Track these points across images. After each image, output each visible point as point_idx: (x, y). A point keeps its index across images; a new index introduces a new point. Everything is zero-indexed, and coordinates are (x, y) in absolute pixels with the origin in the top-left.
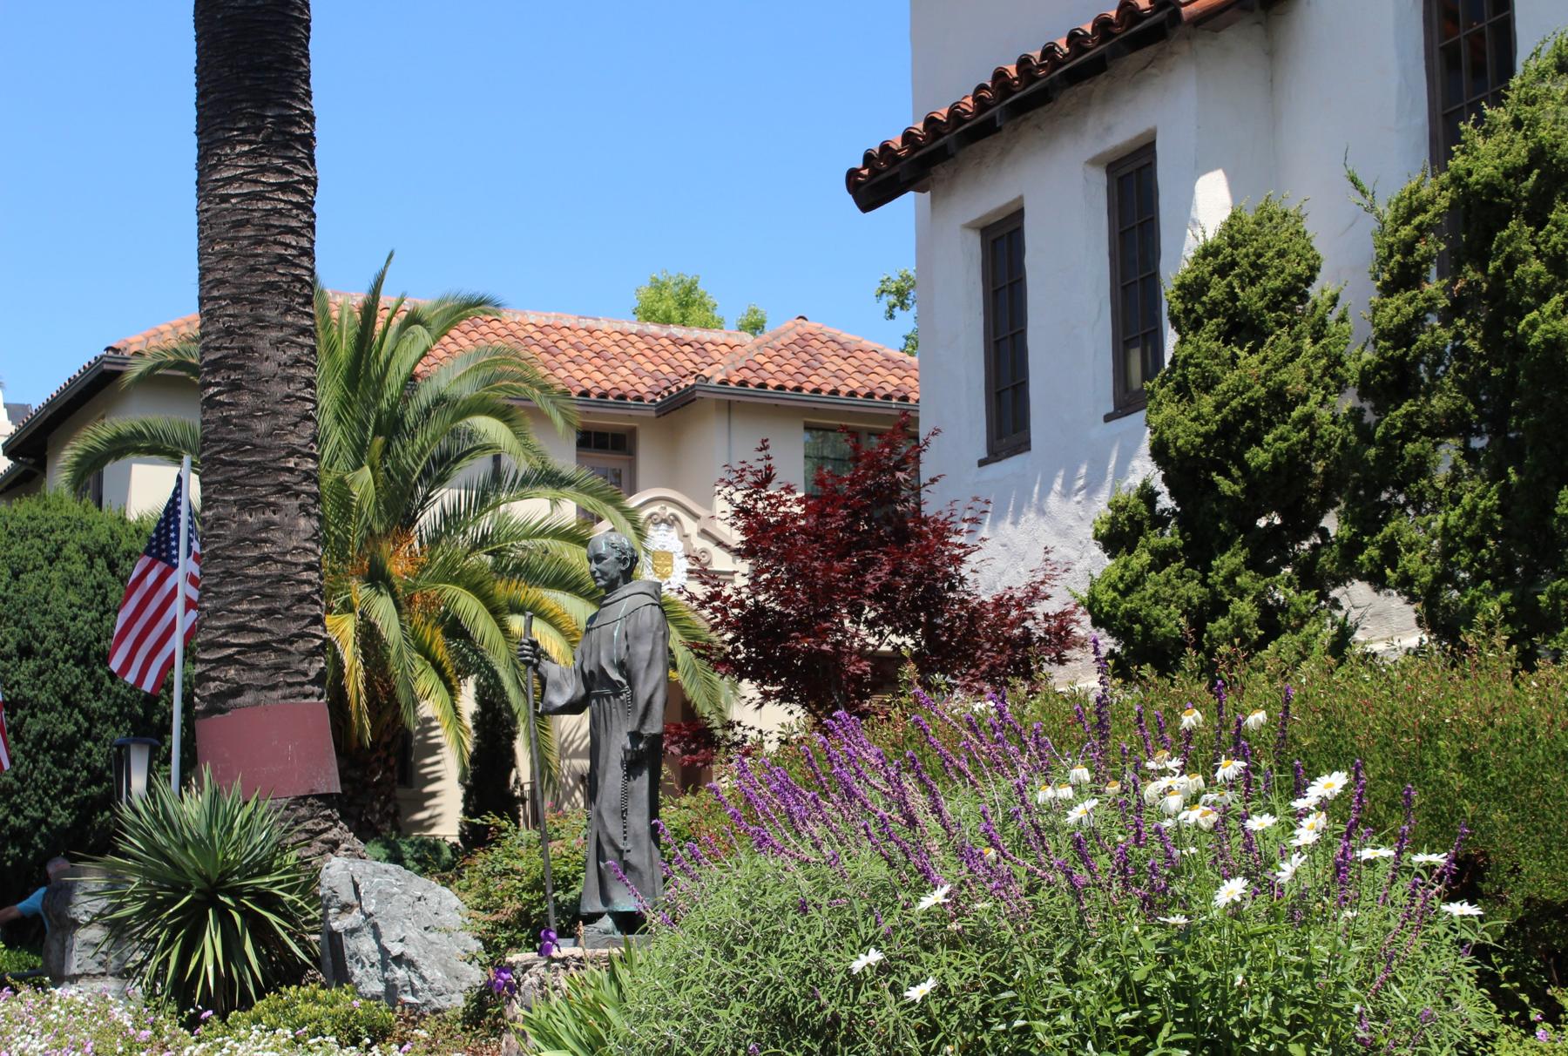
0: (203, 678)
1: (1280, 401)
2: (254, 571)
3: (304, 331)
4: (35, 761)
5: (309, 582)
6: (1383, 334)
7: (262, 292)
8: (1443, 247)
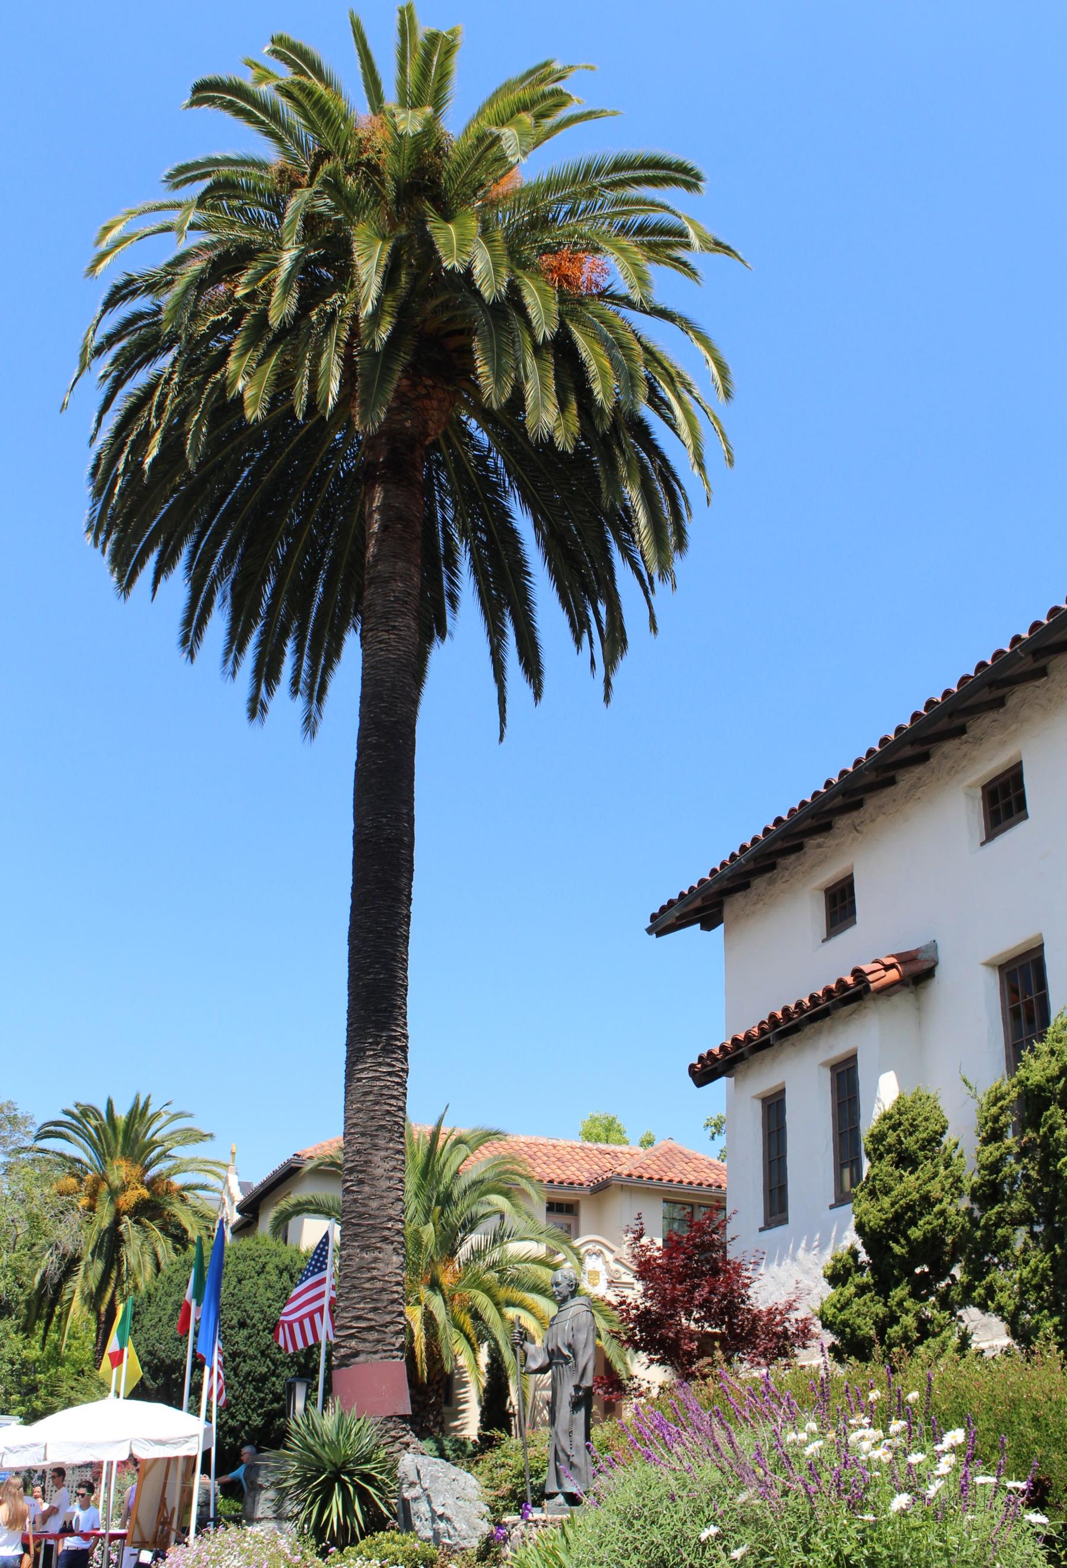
0: (337, 1346)
1: (927, 1202)
2: (367, 1285)
3: (399, 1152)
4: (244, 1388)
5: (397, 1292)
6: (983, 1167)
7: (377, 1130)
8: (1015, 1119)
